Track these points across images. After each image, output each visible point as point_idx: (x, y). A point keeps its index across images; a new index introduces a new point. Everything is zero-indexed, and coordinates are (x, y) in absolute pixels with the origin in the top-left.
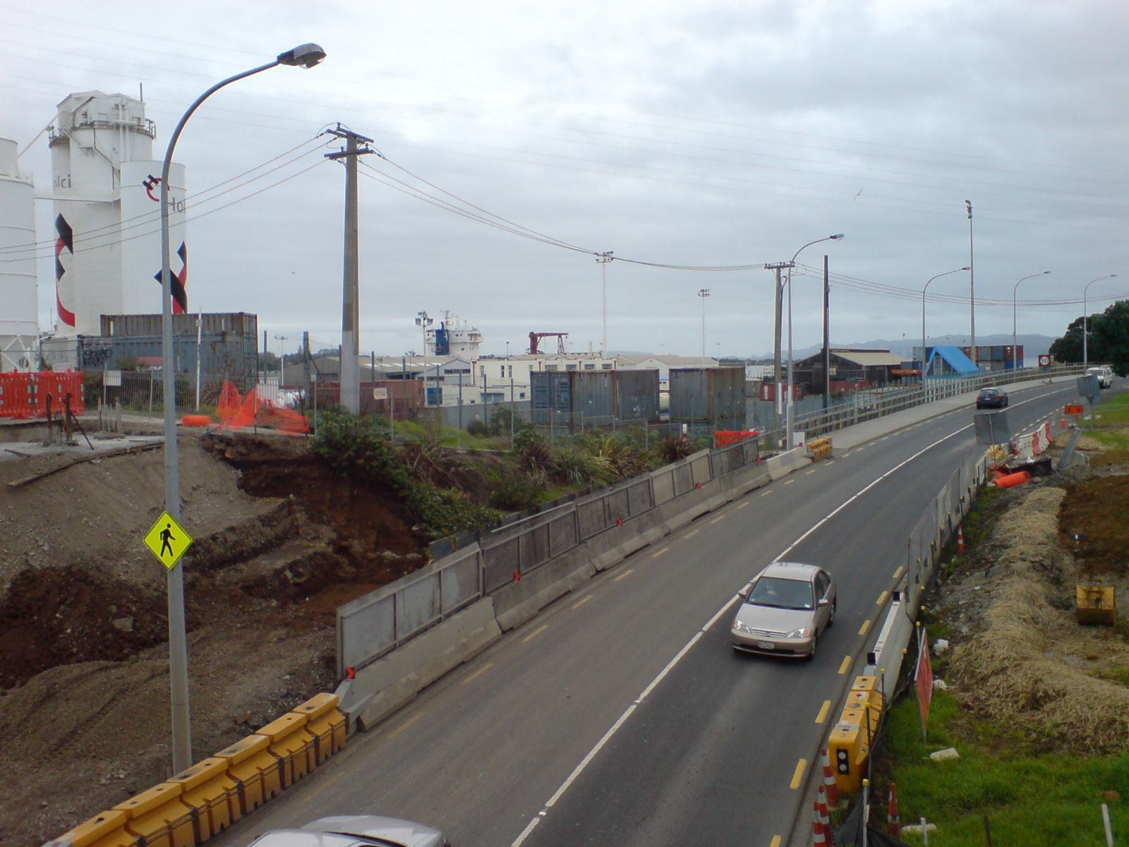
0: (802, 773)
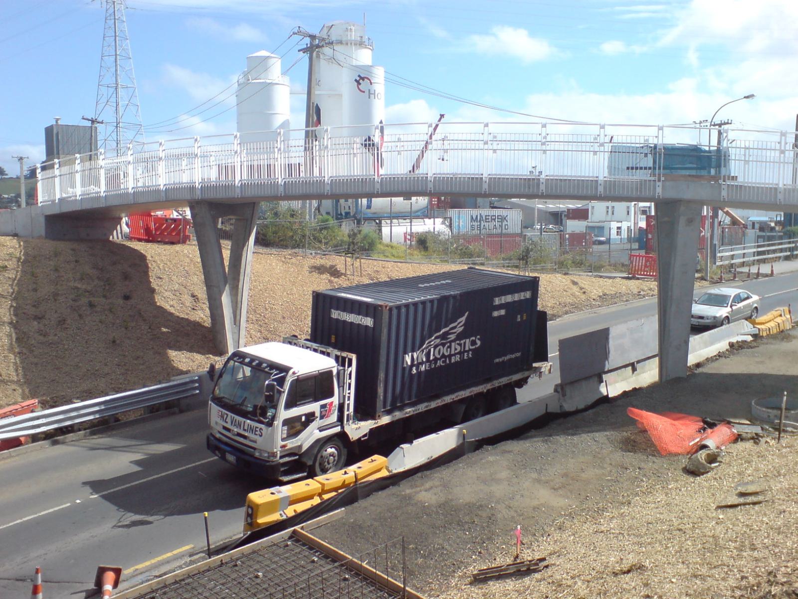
0: (271, 516)
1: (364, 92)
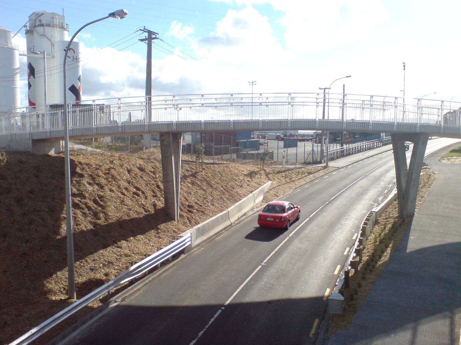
1: (70, 57)
